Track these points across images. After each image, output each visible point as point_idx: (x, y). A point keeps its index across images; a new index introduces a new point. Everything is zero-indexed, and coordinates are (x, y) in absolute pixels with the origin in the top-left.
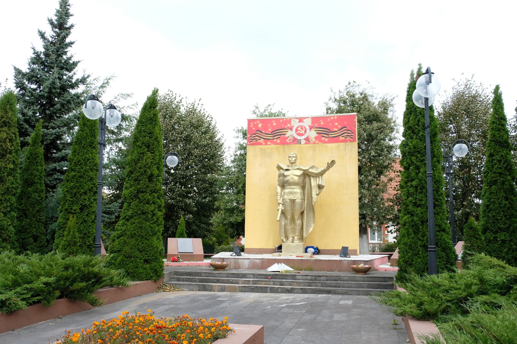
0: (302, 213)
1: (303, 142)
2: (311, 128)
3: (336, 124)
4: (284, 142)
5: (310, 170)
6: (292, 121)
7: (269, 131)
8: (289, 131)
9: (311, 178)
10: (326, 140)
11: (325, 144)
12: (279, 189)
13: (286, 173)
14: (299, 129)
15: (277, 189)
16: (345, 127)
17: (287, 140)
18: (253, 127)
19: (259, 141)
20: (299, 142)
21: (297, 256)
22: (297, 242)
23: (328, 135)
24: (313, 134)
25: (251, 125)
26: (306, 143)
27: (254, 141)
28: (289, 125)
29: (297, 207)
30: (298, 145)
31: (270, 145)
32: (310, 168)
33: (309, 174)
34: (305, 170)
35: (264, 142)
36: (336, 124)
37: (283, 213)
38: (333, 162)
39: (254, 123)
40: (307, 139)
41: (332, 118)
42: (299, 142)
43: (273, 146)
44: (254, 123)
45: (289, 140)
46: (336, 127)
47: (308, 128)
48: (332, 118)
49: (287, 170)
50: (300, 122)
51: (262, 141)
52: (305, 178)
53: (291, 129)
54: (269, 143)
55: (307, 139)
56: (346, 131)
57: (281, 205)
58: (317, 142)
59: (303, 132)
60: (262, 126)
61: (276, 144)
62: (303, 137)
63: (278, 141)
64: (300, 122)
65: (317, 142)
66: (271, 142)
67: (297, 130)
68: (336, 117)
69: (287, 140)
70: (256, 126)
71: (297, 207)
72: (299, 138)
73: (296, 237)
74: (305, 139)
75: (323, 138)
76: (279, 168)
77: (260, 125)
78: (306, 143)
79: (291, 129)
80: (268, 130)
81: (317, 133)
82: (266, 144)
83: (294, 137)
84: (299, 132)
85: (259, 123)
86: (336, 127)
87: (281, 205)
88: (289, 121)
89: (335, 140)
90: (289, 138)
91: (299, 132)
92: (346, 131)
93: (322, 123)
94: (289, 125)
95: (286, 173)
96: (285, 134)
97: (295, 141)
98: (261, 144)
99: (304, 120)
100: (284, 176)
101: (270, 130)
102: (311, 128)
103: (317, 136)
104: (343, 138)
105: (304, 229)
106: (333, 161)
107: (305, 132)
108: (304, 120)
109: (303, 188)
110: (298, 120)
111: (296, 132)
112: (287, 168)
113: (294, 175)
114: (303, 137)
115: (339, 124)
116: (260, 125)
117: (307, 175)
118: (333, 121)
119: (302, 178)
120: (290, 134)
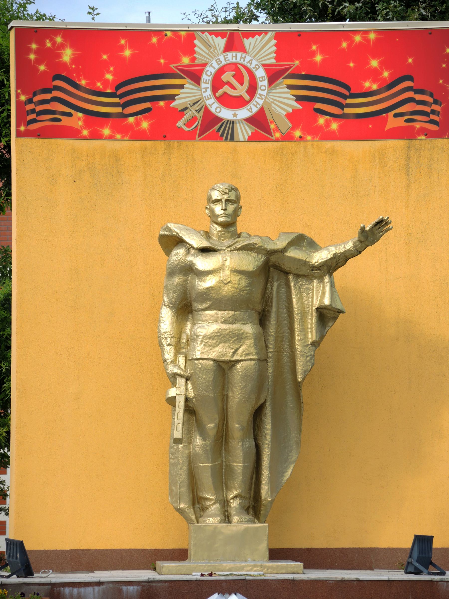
0: (258, 414)
1: (244, 131)
2: (274, 76)
3: (374, 63)
4: (166, 129)
5: (292, 253)
6: (199, 47)
7: (106, 83)
8: (189, 85)
9: (291, 277)
10: (334, 126)
11: (329, 144)
12: (167, 317)
13: (202, 263)
14: (227, 77)
15: (158, 320)
16: (409, 78)
17: (180, 124)
18: (38, 62)
19: (65, 121)
20: (226, 131)
21: (275, 554)
22: (239, 523)
23: (341, 106)
24: (281, 101)
25: (29, 50)
26: (253, 138)
27: (45, 121)
28: (186, 60)
29: (238, 394)
30: (230, 144)
31: (111, 138)
32: (291, 244)
33: (287, 266)
34: (274, 252)
35: (87, 125)
36: (374, 63)
37: (190, 410)
38: (381, 225)
39: (41, 43)
40: (260, 124)
41: (358, 38)
42: (226, 131)
43: (123, 145)
44: (41, 43)
45: (188, 124)
46: (375, 75)
47: (260, 73)
48: (358, 38)
49: (204, 251)
50: (229, 48)
51: (77, 120)
52: (267, 280)
53: (196, 78)
54: (106, 132)
55: (260, 124)
56: (410, 94)
57: (181, 382)
58: (298, 134)
59: (241, 91)
60: (74, 60)
61: (138, 135)
62: (244, 113)
63: (145, 125)
64: (229, 48)
65: (298, 134)
66: (116, 129)
67: (217, 83)
68: (372, 36)
69: (180, 124)
70: (50, 56)
71: (238, 394)
72: (226, 114)
73: (234, 504)
74: (250, 120)
75: (321, 121)
76: (171, 242)
77: (67, 55)
78: (253, 138)
79: (196, 78)
80: (101, 78)
81: (299, 99)
82: (96, 135)
83: (207, 111)
84: (226, 89)
85: (62, 46)
86: (375, 75)
87: (181, 382)
88: (183, 41)
89: (368, 127)
90: (188, 115)
91: (226, 89)
92: (410, 94)
93: (318, 58)
94: (186, 60)
95: (202, 263)
96: (172, 98)
97: (211, 127)
98: (72, 133)
99: (247, 42)
100: (189, 270)
101: (109, 77)
102: (274, 76)
103: (295, 111)
104: (400, 122)
105: (265, 473)
106: (381, 221)
107: (252, 90)
108: (247, 42)
109: (263, 320)
110: (221, 42)
111: (215, 89)
112: (205, 244)
113: (221, 271)
114: (244, 113)
115: (384, 65)
116: (67, 55)
117: (278, 268)
118: (364, 50)
119: (261, 280)
120: (191, 96)
